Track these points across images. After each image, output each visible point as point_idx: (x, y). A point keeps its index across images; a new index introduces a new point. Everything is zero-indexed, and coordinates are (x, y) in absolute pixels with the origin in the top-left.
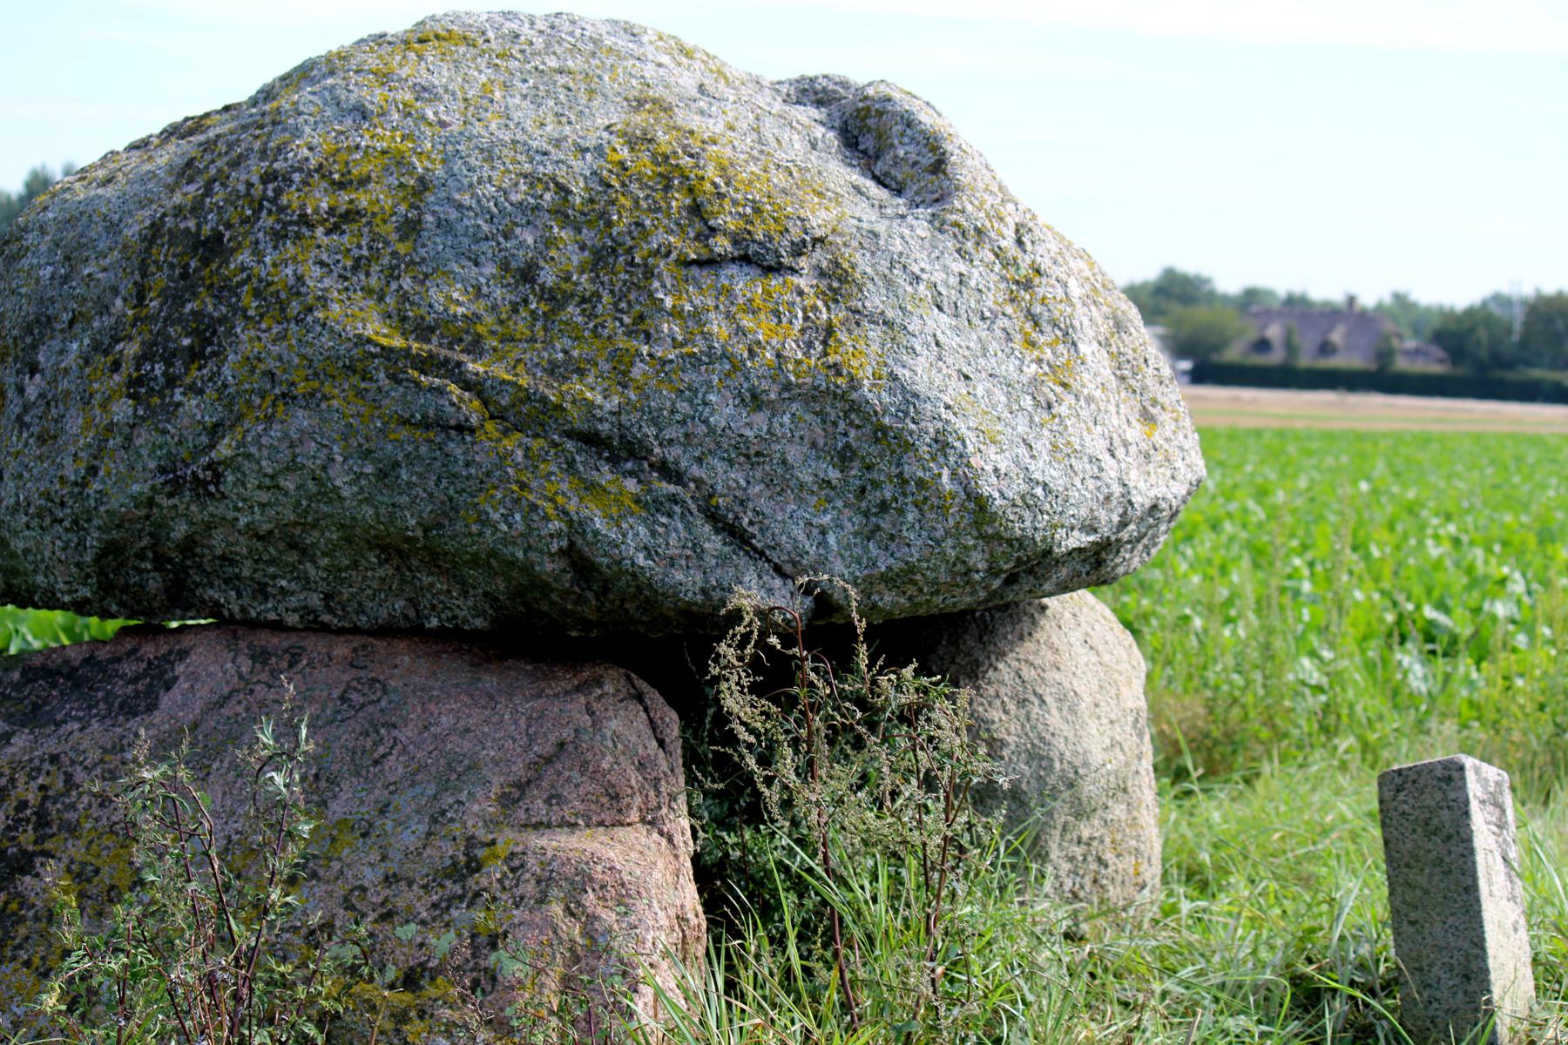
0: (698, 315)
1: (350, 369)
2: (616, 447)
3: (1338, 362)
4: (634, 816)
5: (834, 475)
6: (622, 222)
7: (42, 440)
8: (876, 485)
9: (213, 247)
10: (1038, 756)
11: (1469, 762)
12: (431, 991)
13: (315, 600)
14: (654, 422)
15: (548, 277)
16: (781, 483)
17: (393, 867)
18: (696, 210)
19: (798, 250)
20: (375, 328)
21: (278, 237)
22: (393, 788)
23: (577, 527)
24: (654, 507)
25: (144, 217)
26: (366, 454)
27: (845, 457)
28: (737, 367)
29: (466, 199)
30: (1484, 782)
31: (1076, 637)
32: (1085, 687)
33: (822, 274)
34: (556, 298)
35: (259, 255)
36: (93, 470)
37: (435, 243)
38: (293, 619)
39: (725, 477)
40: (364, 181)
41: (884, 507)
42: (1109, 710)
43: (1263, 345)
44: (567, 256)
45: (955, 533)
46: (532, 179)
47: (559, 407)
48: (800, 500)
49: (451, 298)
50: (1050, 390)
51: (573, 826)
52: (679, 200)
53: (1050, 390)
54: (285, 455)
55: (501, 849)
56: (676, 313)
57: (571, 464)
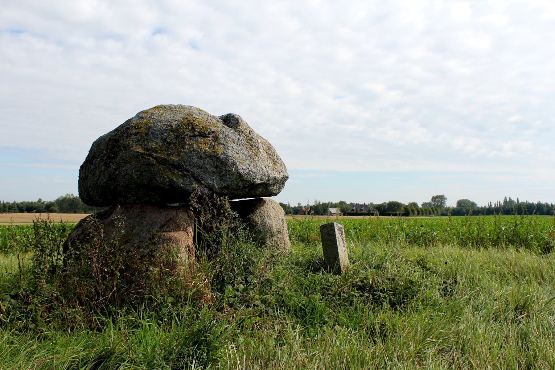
0: (192, 145)
1: (136, 157)
2: (179, 167)
3: (363, 212)
4: (182, 229)
5: (215, 170)
6: (181, 131)
7: (93, 175)
8: (222, 172)
9: (117, 141)
10: (264, 225)
11: (335, 223)
12: (144, 259)
13: (135, 198)
14: (184, 162)
15: (168, 140)
16: (206, 172)
17: (141, 240)
18: (193, 128)
19: (209, 134)
20: (140, 150)
21: (127, 137)
22: (144, 227)
23: (171, 180)
24: (184, 176)
25: (109, 138)
26: (138, 171)
27: (216, 167)
28: (198, 152)
29: (156, 129)
30: (338, 227)
31: (271, 207)
32: (272, 215)
33: (213, 137)
34: (169, 144)
35: (124, 141)
36: (99, 179)
37: (151, 136)
38: (132, 202)
39: (196, 171)
40: (141, 128)
41: (223, 175)
42: (276, 218)
43: (353, 210)
44: (172, 136)
45: (236, 179)
46: (167, 125)
47: (168, 160)
48: (209, 175)
49: (153, 145)
50: (254, 156)
51: (171, 231)
52: (190, 127)
53: (254, 156)
54: (126, 172)
55: (158, 235)
56: (188, 144)
57: (170, 170)
